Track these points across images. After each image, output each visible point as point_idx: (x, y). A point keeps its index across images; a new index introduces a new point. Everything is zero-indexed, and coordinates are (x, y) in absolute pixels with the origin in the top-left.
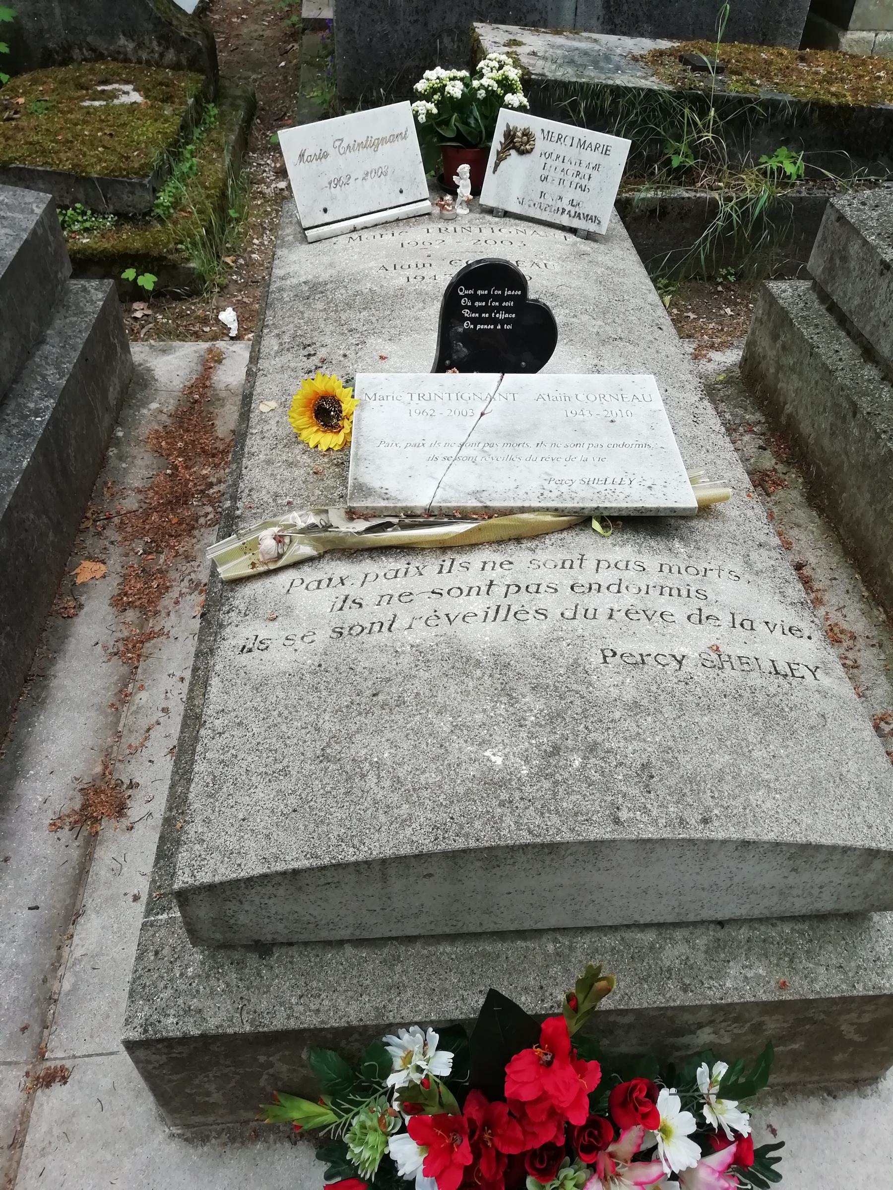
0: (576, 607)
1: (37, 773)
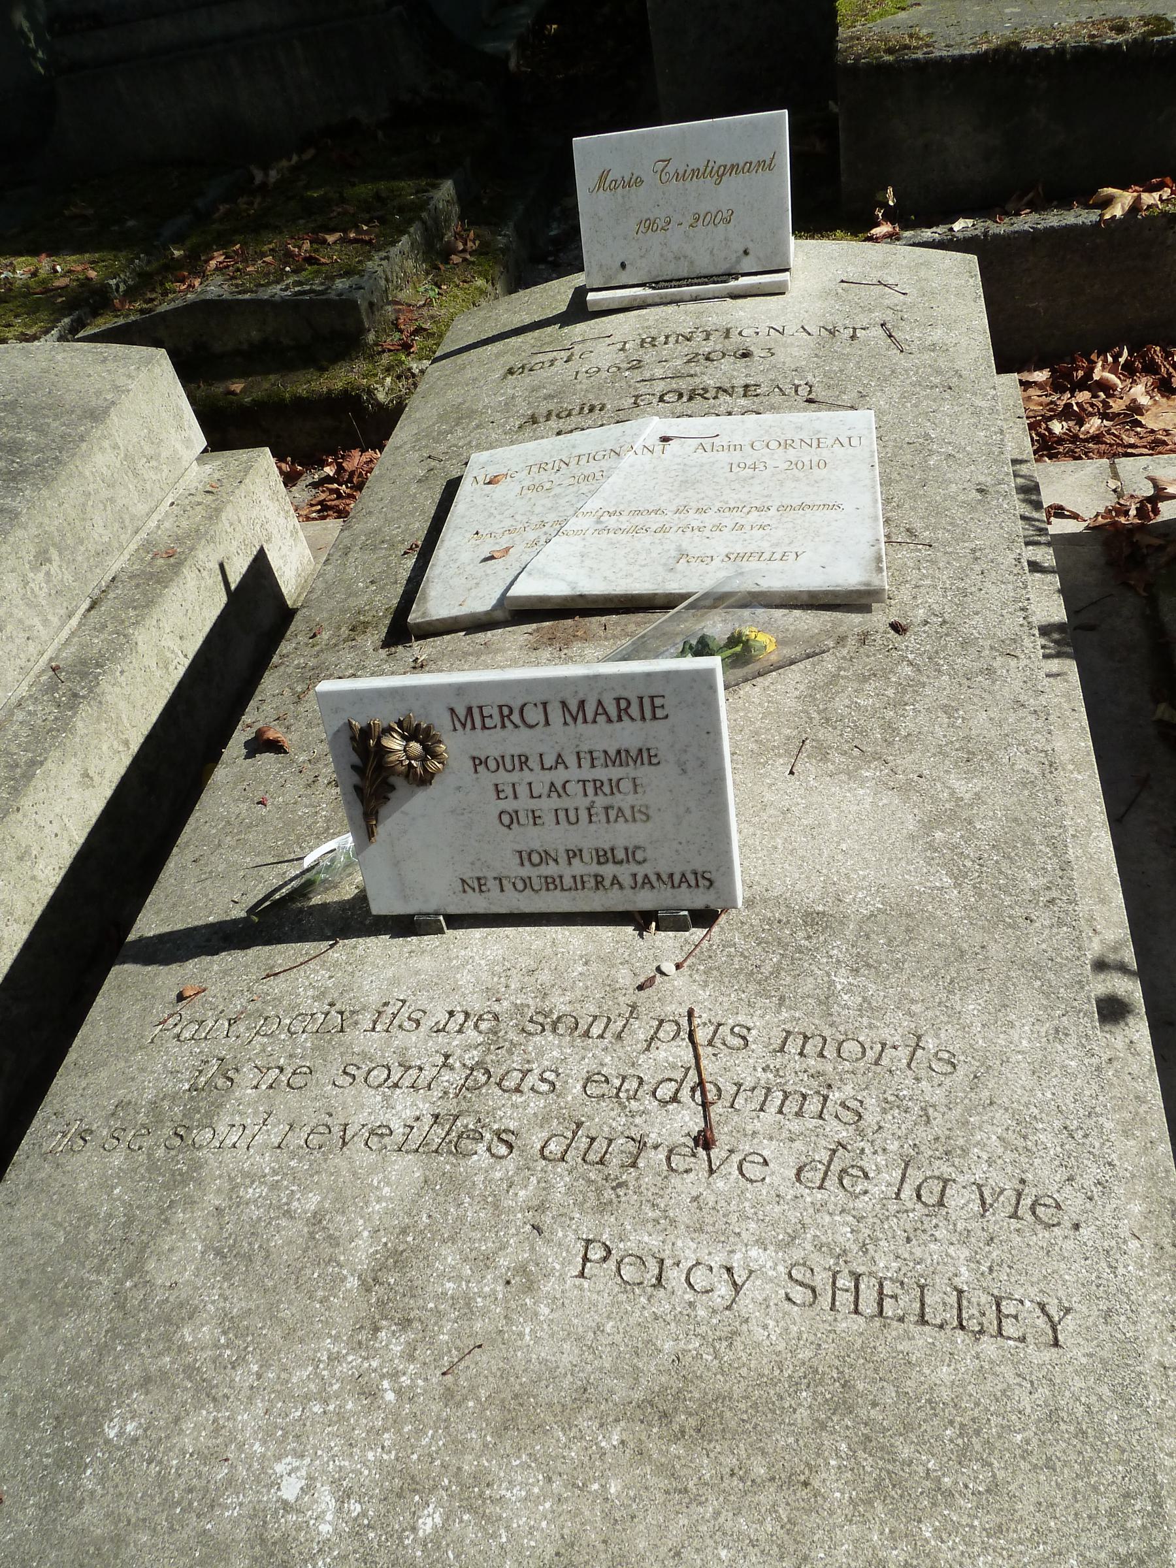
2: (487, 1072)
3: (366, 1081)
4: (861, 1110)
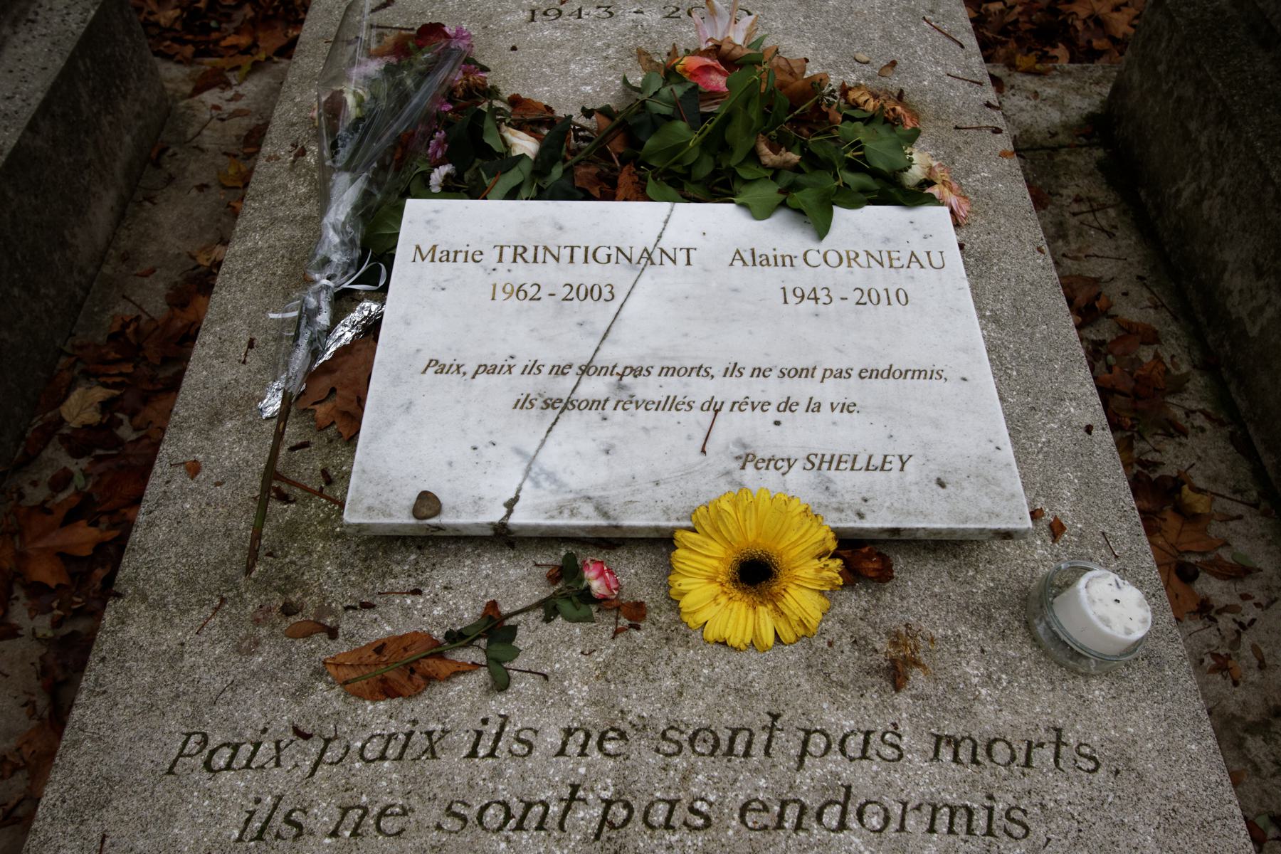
2: (627, 805)
3: (481, 823)
4: (1025, 820)
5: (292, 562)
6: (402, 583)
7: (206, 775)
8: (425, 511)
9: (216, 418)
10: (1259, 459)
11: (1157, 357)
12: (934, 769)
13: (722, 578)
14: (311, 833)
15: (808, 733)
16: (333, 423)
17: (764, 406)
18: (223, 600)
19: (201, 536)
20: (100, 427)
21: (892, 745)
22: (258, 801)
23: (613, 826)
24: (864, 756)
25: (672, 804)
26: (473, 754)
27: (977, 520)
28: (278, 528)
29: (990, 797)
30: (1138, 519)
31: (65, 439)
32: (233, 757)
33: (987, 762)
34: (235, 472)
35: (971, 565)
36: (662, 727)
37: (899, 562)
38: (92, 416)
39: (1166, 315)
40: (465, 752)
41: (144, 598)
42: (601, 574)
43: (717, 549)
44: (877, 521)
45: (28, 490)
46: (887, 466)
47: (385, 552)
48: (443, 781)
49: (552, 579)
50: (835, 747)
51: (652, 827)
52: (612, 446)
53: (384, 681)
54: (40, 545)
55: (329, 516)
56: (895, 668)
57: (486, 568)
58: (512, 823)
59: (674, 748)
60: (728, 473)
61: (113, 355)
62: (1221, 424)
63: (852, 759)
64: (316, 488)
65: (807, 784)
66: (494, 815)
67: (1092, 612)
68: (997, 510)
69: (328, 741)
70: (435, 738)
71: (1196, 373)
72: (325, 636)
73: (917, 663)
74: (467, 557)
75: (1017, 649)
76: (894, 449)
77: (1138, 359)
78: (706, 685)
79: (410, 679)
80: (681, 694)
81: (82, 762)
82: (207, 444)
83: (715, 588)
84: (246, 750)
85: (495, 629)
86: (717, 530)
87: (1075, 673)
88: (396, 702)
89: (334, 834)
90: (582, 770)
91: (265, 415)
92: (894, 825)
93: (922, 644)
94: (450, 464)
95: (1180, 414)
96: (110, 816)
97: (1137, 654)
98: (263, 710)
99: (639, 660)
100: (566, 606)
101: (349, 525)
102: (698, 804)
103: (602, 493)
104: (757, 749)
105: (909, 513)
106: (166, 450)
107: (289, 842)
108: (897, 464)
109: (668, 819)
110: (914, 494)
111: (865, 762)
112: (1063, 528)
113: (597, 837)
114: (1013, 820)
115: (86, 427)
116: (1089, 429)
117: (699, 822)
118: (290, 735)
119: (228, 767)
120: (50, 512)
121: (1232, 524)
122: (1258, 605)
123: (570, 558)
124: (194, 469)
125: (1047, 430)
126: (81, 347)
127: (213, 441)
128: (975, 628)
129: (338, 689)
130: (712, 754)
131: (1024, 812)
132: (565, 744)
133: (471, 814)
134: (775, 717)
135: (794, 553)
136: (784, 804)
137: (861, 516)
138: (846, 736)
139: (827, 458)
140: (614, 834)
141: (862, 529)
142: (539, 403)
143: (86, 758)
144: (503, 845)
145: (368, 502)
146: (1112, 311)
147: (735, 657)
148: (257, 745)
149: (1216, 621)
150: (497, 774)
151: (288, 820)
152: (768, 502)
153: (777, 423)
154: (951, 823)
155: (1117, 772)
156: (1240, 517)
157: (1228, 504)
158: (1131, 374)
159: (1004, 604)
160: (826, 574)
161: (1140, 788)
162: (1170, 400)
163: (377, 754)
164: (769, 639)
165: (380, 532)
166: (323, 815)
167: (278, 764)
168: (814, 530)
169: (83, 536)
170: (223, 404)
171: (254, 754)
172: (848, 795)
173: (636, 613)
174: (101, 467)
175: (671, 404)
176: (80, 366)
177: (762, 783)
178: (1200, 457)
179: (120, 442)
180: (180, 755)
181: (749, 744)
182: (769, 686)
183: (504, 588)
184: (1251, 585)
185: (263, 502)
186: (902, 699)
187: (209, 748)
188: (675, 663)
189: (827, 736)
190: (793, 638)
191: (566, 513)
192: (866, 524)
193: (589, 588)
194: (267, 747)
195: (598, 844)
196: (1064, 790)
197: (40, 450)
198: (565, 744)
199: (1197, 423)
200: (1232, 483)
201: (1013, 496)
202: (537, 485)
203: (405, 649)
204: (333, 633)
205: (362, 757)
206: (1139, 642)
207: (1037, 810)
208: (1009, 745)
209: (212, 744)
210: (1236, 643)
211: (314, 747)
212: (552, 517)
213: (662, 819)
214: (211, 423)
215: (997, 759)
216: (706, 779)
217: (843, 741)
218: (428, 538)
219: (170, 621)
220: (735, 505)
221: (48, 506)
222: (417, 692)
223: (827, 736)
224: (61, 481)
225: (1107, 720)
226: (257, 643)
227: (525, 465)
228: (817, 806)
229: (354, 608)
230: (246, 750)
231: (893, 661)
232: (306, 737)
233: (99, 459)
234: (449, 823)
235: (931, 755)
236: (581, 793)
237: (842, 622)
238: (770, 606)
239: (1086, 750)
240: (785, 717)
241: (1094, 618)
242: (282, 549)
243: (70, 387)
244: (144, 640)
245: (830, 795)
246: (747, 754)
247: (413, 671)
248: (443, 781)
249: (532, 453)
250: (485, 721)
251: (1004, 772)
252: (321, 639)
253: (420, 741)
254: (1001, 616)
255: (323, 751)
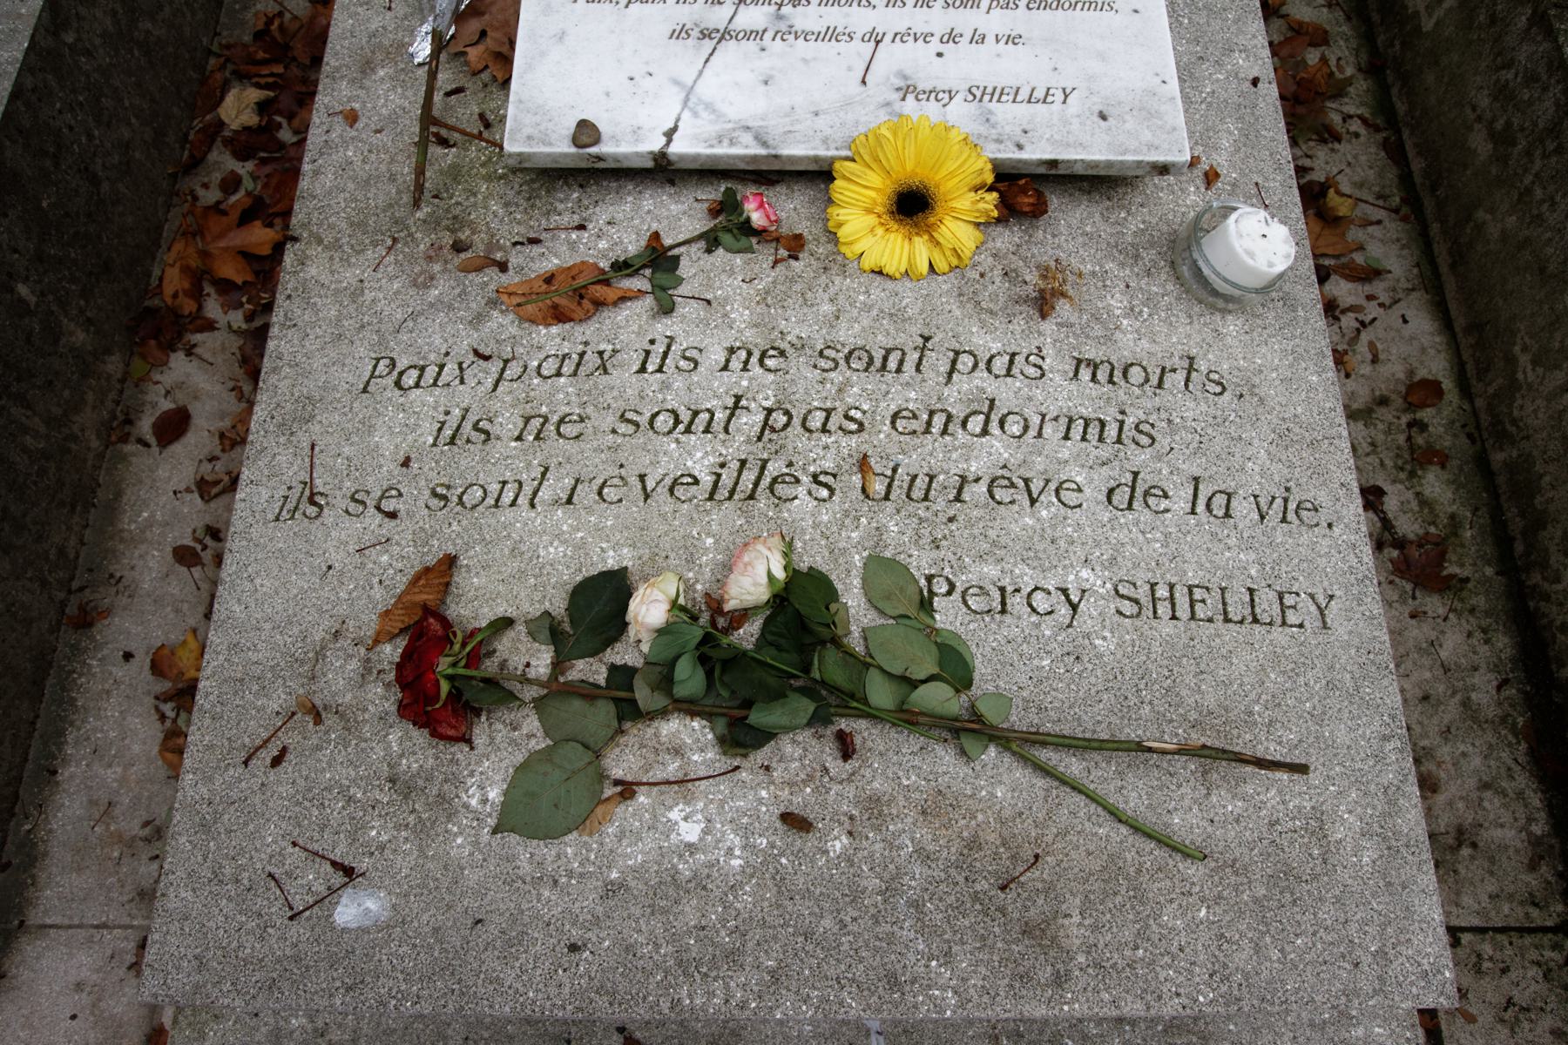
0: (895, 470)
1: (152, 515)
2: (787, 413)
5: (458, 203)
6: (566, 219)
7: (398, 392)
8: (585, 139)
9: (367, 67)
10: (1408, 165)
11: (1324, 60)
12: (1073, 386)
13: (880, 209)
14: (498, 438)
15: (957, 353)
16: (486, 67)
17: (927, 37)
18: (395, 240)
19: (367, 182)
20: (260, 130)
21: (1035, 365)
22: (447, 413)
23: (773, 430)
24: (1009, 374)
25: (829, 412)
26: (643, 369)
27: (1135, 152)
28: (441, 172)
29: (1123, 412)
30: (1293, 172)
31: (228, 142)
32: (420, 377)
33: (1123, 383)
34: (393, 119)
35: (1124, 207)
36: (819, 347)
37: (1054, 201)
38: (251, 118)
39: (1340, 15)
40: (635, 368)
41: (320, 241)
42: (761, 206)
43: (875, 179)
44: (1036, 152)
45: (201, 192)
46: (1050, 99)
47: (548, 191)
48: (615, 393)
49: (714, 212)
50: (982, 365)
51: (810, 431)
52: (771, 77)
53: (555, 307)
54: (222, 244)
55: (490, 159)
56: (1043, 298)
57: (647, 204)
58: (681, 427)
59: (830, 364)
60: (888, 104)
61: (261, 55)
62: (1377, 129)
63: (997, 377)
64: (475, 132)
65: (955, 396)
66: (664, 422)
67: (1238, 245)
68: (1157, 142)
69: (506, 362)
70: (606, 356)
71: (1360, 76)
72: (496, 269)
73: (1064, 295)
74: (629, 193)
75: (1162, 286)
76: (1058, 82)
77: (1304, 61)
78: (861, 310)
79: (579, 304)
80: (838, 318)
81: (284, 386)
82: (362, 93)
83: (872, 220)
84: (431, 371)
85: (659, 259)
86: (877, 160)
87: (1213, 309)
88: (567, 326)
89: (519, 438)
90: (745, 383)
91: (416, 61)
92: (1032, 432)
93: (1071, 278)
94: (608, 94)
95: (1336, 119)
96: (316, 428)
97: (1271, 289)
98: (442, 335)
99: (798, 287)
100: (726, 238)
101: (510, 155)
102: (852, 413)
103: (762, 123)
104: (909, 366)
105: (1068, 145)
106: (322, 100)
107: (479, 446)
108: (1059, 96)
109: (825, 424)
110: (1075, 126)
111: (1009, 380)
112: (1217, 175)
113: (759, 439)
114: (1141, 432)
115: (247, 129)
116: (1255, 82)
117: (854, 427)
118: (471, 357)
119: (417, 385)
120: (225, 213)
121: (1370, 229)
122: (1381, 305)
123: (729, 193)
124: (352, 118)
125: (1214, 79)
126: (228, 47)
127: (368, 90)
128: (1122, 265)
129: (511, 316)
130: (866, 370)
131: (1152, 425)
132: (728, 361)
133: (643, 420)
134: (927, 339)
135: (950, 184)
136: (932, 413)
137: (1020, 147)
138: (992, 357)
139: (989, 90)
140: (774, 436)
141: (1020, 161)
142: (695, 33)
143: (287, 382)
144: (673, 446)
145: (527, 131)
146: (1284, 10)
147: (889, 285)
148: (441, 367)
149: (1338, 319)
150: (665, 386)
151: (476, 427)
152: (928, 130)
153: (940, 55)
154: (1085, 432)
155: (1241, 396)
156: (1379, 222)
157: (1369, 209)
158: (1294, 77)
159: (1152, 245)
160: (981, 205)
161: (1260, 410)
162: (1329, 104)
163: (553, 372)
164: (924, 268)
165: (541, 165)
166: (507, 423)
167: (462, 382)
168: (972, 160)
169: (259, 236)
170: (373, 52)
171: (439, 374)
172: (991, 407)
173: (795, 245)
174: (267, 169)
175: (831, 34)
176: (230, 67)
177: (913, 395)
178: (1354, 163)
179: (282, 146)
180: (372, 376)
181: (901, 362)
182: (922, 311)
183: (665, 222)
184: (1379, 288)
185: (422, 145)
186: (1048, 326)
187: (398, 370)
188: (832, 290)
189: (975, 356)
190: (947, 269)
191: (726, 142)
192: (1024, 155)
193: (748, 220)
194: (451, 368)
195: (760, 445)
196: (1190, 408)
197: (206, 154)
198: (728, 361)
199: (1353, 128)
200: (1377, 189)
201: (1174, 129)
202: (695, 114)
203: (573, 278)
204: (503, 267)
205: (539, 374)
206: (1281, 276)
207: (1164, 424)
208: (1145, 369)
209: (400, 367)
210: (1354, 340)
211: (494, 367)
212: (712, 146)
213: (819, 425)
214: (363, 72)
215: (1132, 380)
216: (860, 391)
217: (989, 361)
218: (588, 173)
219: (347, 260)
220: (895, 134)
221: (222, 207)
222: (587, 318)
223: (975, 356)
224: (231, 184)
225: (1238, 352)
226: (432, 278)
227: (683, 95)
228: (962, 415)
229: (522, 244)
230: (431, 371)
231: (1042, 291)
232: (487, 358)
233: (264, 162)
234: (623, 428)
235: (1071, 375)
236: (744, 403)
237: (995, 256)
238: (926, 237)
239: (1215, 377)
240: (936, 339)
241: (1240, 250)
242: (447, 191)
243: (225, 88)
244: (325, 278)
245: (975, 406)
246: (899, 370)
247: (582, 297)
248: (615, 393)
249: (690, 83)
250: (652, 342)
251: (1137, 391)
252: (493, 272)
253: (592, 360)
254: (1148, 256)
255: (503, 370)
